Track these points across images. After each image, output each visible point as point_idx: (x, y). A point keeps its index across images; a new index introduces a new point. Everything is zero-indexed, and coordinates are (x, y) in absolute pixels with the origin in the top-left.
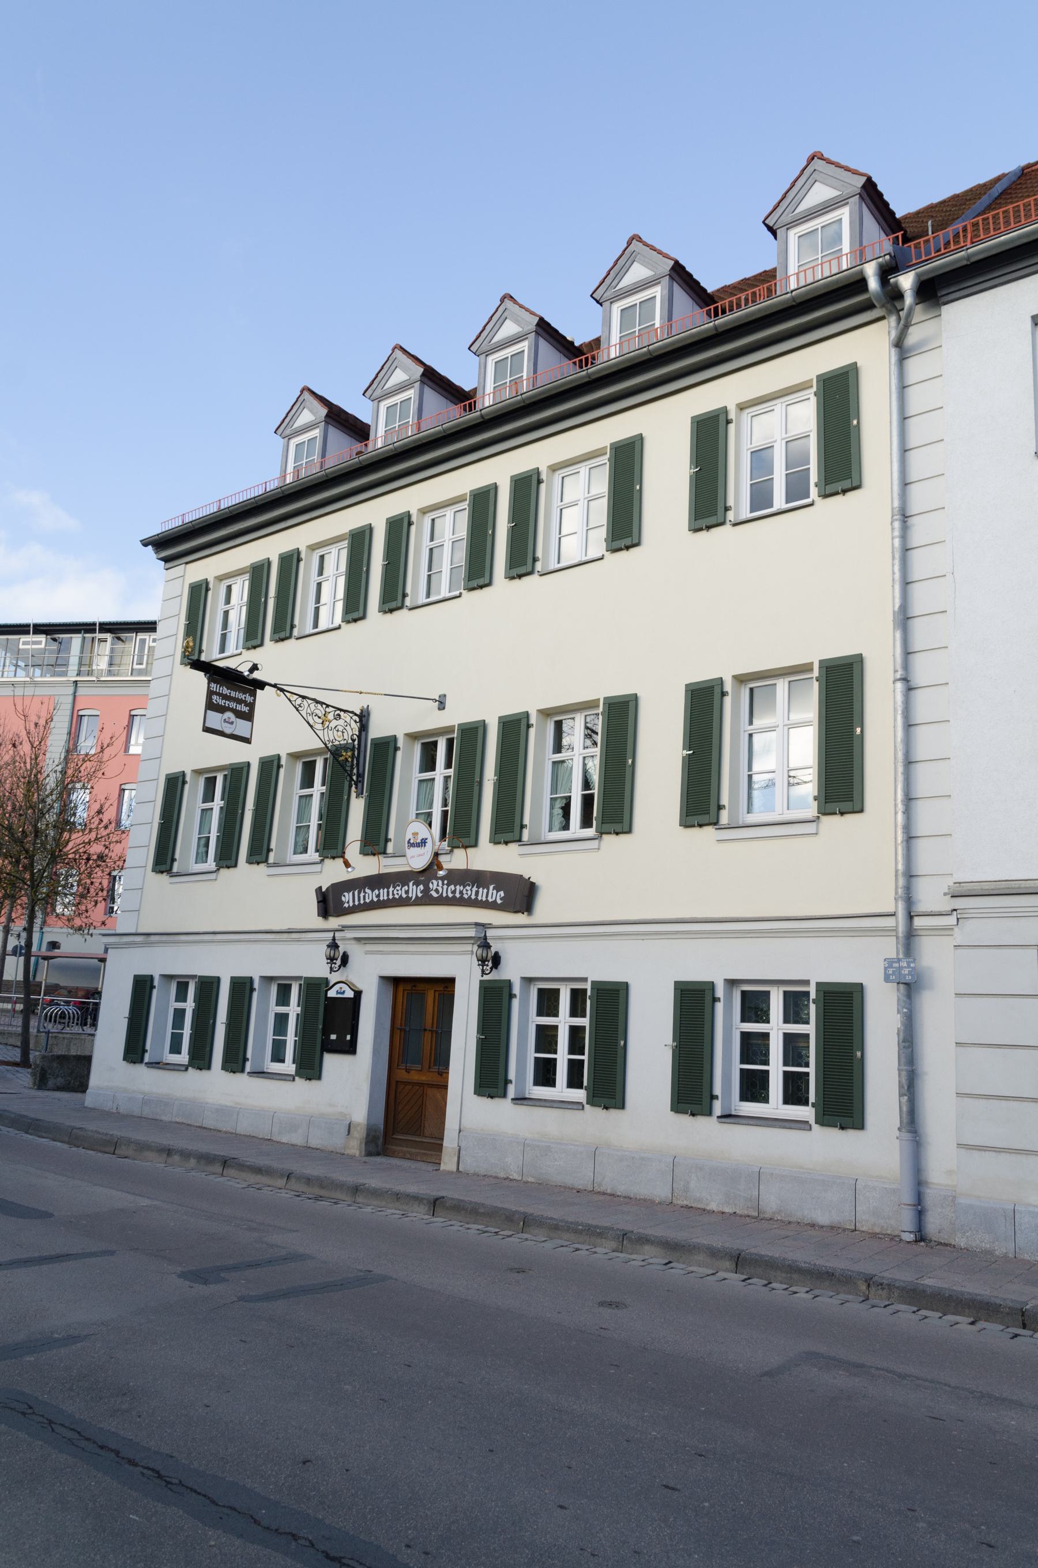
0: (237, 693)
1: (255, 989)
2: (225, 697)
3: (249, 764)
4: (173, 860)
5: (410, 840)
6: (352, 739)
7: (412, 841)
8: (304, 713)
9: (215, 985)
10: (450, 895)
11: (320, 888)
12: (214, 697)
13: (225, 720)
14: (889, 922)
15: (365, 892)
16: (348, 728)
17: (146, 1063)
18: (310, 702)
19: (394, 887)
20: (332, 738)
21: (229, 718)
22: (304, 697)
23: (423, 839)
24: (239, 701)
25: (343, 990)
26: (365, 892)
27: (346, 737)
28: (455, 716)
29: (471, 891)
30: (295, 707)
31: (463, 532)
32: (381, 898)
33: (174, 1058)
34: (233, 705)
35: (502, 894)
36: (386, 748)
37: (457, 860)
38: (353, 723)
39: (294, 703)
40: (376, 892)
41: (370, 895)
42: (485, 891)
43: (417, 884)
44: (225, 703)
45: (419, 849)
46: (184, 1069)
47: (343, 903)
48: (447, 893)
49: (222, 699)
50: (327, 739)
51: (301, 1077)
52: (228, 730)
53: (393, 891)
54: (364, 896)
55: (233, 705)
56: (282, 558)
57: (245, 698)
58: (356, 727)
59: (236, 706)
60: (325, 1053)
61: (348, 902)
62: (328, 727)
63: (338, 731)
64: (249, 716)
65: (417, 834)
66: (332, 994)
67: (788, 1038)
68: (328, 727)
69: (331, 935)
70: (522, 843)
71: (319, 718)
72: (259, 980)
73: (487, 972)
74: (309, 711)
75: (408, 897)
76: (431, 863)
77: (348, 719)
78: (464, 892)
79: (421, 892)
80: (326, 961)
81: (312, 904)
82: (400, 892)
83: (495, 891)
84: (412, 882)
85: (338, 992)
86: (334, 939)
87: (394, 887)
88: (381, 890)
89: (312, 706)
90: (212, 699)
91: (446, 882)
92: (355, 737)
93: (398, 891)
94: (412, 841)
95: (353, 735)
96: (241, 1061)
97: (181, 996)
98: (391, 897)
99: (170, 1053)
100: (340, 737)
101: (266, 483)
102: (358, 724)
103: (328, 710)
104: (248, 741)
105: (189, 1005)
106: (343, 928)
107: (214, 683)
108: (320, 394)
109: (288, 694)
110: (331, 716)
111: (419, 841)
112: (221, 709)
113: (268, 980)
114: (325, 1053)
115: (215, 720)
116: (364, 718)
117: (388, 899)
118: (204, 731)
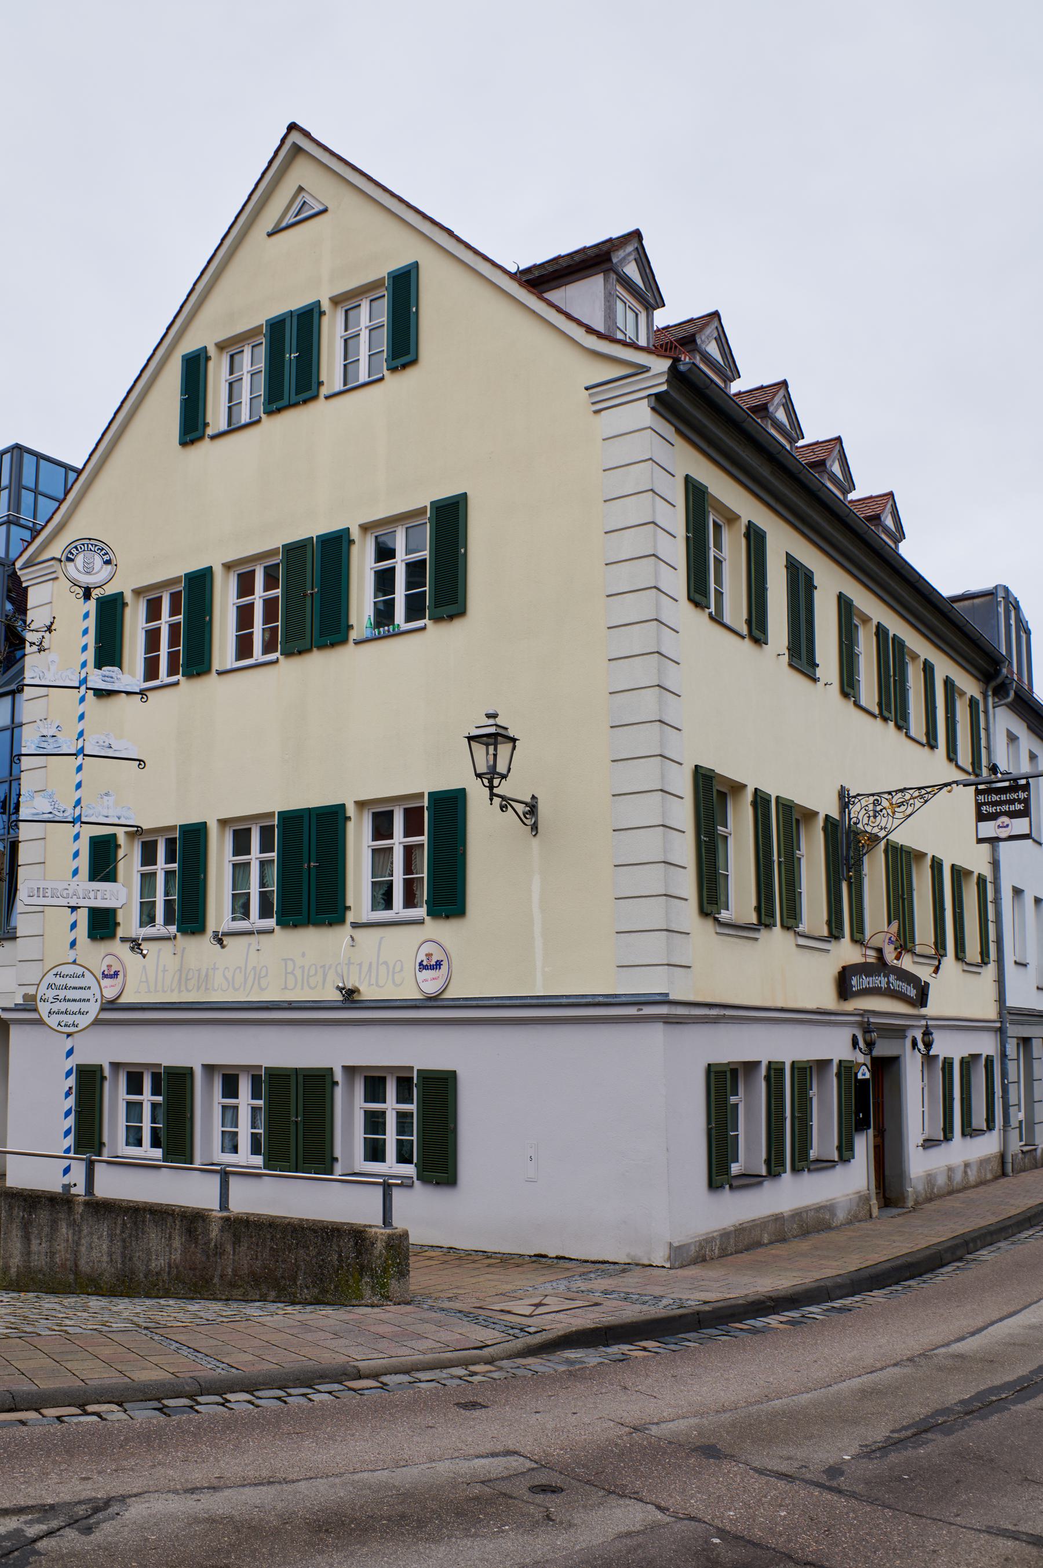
1: (106, 1077)
5: (422, 961)
13: (999, 826)
21: (1003, 823)
23: (438, 961)
30: (878, 794)
31: (383, 318)
34: (1005, 808)
44: (996, 810)
47: (852, 986)
55: (1005, 808)
57: (1018, 796)
59: (1009, 808)
67: (399, 1143)
97: (230, 1088)
107: (981, 795)
111: (433, 963)
112: (992, 817)
115: (988, 829)
118: (977, 843)
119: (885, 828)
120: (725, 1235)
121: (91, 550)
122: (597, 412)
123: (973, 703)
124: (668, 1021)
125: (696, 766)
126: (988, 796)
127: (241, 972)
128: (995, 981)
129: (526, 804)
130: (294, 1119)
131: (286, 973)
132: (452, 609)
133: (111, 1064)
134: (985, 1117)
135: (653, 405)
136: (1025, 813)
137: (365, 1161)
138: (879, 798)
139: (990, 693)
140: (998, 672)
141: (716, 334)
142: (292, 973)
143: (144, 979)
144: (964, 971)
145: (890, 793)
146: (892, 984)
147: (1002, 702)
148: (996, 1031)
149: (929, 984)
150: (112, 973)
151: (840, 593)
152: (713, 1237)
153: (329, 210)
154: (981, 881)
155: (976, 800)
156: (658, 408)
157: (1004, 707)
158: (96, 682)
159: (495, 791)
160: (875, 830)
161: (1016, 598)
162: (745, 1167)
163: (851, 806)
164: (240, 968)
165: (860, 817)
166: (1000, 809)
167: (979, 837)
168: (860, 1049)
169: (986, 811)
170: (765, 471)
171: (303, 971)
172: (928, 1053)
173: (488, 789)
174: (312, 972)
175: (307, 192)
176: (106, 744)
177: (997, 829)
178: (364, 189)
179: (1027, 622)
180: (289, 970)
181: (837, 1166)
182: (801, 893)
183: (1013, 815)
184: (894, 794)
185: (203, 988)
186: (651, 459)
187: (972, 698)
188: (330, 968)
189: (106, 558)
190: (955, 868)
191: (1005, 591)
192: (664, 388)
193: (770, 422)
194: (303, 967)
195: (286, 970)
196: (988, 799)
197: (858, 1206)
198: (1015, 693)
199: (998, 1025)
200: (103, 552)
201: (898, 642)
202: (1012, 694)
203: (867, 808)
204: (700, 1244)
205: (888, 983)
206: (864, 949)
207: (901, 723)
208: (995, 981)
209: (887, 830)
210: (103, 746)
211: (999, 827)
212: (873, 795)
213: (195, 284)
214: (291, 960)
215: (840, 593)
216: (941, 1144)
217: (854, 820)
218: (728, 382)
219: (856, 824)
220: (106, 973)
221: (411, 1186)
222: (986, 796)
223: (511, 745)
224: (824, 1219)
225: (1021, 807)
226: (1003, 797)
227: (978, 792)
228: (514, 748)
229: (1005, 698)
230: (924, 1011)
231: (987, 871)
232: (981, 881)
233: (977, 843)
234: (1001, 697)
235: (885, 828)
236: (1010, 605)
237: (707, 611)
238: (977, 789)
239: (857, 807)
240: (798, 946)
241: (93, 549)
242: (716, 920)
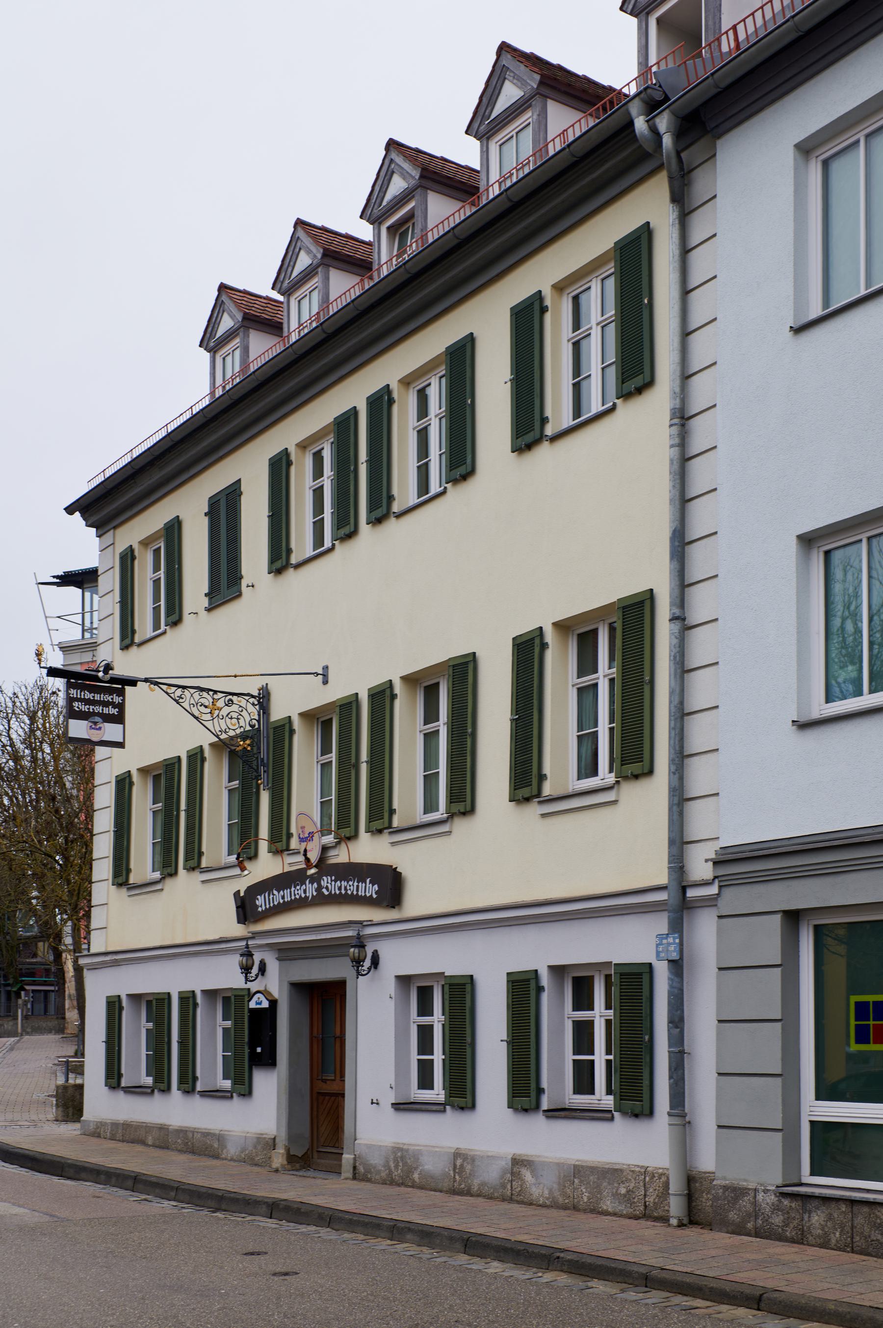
0: (102, 695)
2: (88, 702)
3: (179, 758)
4: (392, 812)
6: (250, 726)
8: (186, 705)
9: (646, 978)
10: (338, 892)
11: (239, 891)
12: (76, 704)
14: (662, 896)
16: (244, 713)
17: (544, 1111)
18: (192, 691)
19: (295, 887)
20: (224, 727)
22: (184, 687)
24: (106, 704)
25: (260, 1000)
26: (273, 895)
27: (242, 723)
28: (335, 692)
29: (353, 885)
30: (175, 700)
32: (286, 900)
33: (426, 1095)
34: (99, 709)
35: (376, 887)
36: (284, 730)
37: (340, 856)
38: (249, 705)
39: (172, 695)
40: (281, 893)
41: (277, 897)
42: (364, 885)
43: (312, 882)
44: (89, 709)
46: (149, 1090)
47: (257, 907)
48: (335, 890)
49: (85, 705)
50: (218, 729)
51: (624, 1113)
53: (294, 891)
54: (273, 898)
55: (99, 709)
56: (371, 403)
57: (112, 699)
58: (254, 711)
59: (103, 710)
60: (254, 1067)
61: (261, 906)
62: (218, 716)
63: (231, 718)
64: (119, 719)
66: (252, 1005)
68: (218, 716)
69: (244, 943)
70: (291, 852)
71: (206, 707)
72: (201, 995)
73: (363, 973)
74: (192, 702)
75: (306, 896)
76: (320, 858)
77: (243, 703)
78: (348, 888)
79: (316, 891)
80: (351, 964)
82: (352, 888)
83: (371, 885)
84: (308, 880)
85: (257, 1003)
86: (247, 946)
87: (295, 887)
88: (285, 891)
89: (196, 696)
90: (73, 706)
91: (333, 878)
92: (254, 721)
93: (298, 890)
95: (251, 720)
96: (533, 1094)
97: (583, 1000)
98: (293, 898)
99: (818, 1098)
100: (234, 725)
101: (734, 28)
102: (257, 707)
103: (216, 697)
104: (121, 745)
105: (437, 1019)
106: (255, 935)
107: (74, 689)
108: (527, 49)
109: (164, 687)
110: (221, 703)
113: (558, 971)
114: (254, 1067)
116: (263, 699)
120: (115, 1125)
136: (119, 719)
146: (327, 888)
150: (307, 835)
152: (106, 1123)
169: (78, 707)
177: (89, 730)
196: (81, 695)
197: (255, 1147)
204: (97, 1125)
220: (301, 836)
221: (612, 1119)
222: (79, 691)
224: (212, 1146)
226: (97, 697)
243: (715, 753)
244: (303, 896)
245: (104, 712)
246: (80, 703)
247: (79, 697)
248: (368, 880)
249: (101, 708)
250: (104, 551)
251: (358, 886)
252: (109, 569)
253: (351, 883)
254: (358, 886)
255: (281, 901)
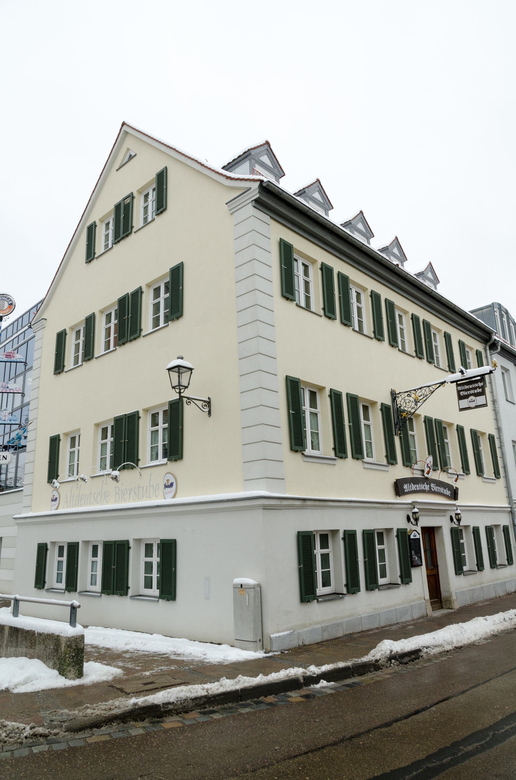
5: (165, 484)
7: (166, 485)
15: (411, 485)
21: (472, 399)
23: (171, 483)
26: (411, 485)
34: (472, 392)
41: (414, 487)
44: (468, 393)
45: (169, 488)
47: (404, 489)
52: (473, 405)
54: (411, 487)
55: (472, 392)
57: (478, 385)
59: (474, 392)
61: (406, 489)
65: (169, 480)
81: (391, 491)
87: (421, 484)
90: (460, 394)
94: (166, 485)
98: (420, 489)
107: (459, 386)
111: (169, 484)
112: (466, 397)
115: (464, 403)
117: (408, 491)
118: (460, 411)
119: (414, 408)
121: (3, 300)
122: (232, 214)
123: (478, 354)
124: (265, 508)
125: (287, 376)
126: (463, 387)
127: (100, 495)
128: (505, 487)
129: (204, 401)
130: (113, 567)
131: (116, 494)
132: (177, 315)
133: (51, 542)
134: (506, 558)
135: (254, 205)
137: (145, 588)
138: (410, 393)
139: (488, 348)
140: (490, 338)
141: (318, 189)
142: (118, 494)
143: (66, 501)
144: (483, 482)
145: (415, 390)
146: (433, 488)
147: (495, 352)
148: (509, 513)
149: (458, 488)
151: (386, 298)
153: (137, 155)
154: (491, 438)
155: (457, 389)
156: (256, 206)
157: (496, 354)
158: (3, 358)
159: (182, 395)
160: (409, 409)
161: (506, 309)
162: (335, 589)
163: (397, 399)
164: (99, 493)
165: (402, 404)
166: (470, 393)
167: (460, 408)
168: (412, 523)
169: (463, 394)
170: (329, 238)
171: (122, 492)
172: (459, 524)
173: (178, 394)
174: (125, 493)
175: (132, 151)
176: (6, 386)
178: (178, 159)
179: (514, 320)
180: (117, 492)
181: (400, 587)
182: (306, 430)
183: (476, 395)
184: (417, 390)
185: (86, 504)
186: (253, 230)
187: (477, 351)
188: (132, 490)
189: (10, 302)
190: (472, 430)
191: (499, 305)
192: (258, 196)
193: (353, 229)
194: (122, 490)
195: (116, 492)
198: (501, 347)
199: (510, 509)
200: (9, 300)
201: (426, 322)
202: (499, 348)
203: (404, 399)
205: (430, 488)
206: (412, 470)
207: (430, 360)
208: (505, 487)
209: (415, 409)
210: (5, 388)
211: (470, 402)
212: (407, 392)
213: (91, 197)
214: (118, 487)
215: (386, 298)
216: (476, 573)
217: (399, 405)
218: (327, 210)
219: (400, 407)
222: (462, 387)
223: (190, 372)
225: (480, 390)
226: (471, 386)
227: (458, 385)
228: (191, 373)
229: (496, 350)
230: (457, 503)
231: (494, 433)
232: (491, 438)
233: (460, 411)
234: (494, 350)
235: (414, 408)
236: (502, 311)
237: (295, 303)
238: (457, 384)
239: (400, 399)
240: (365, 468)
241: (4, 299)
242: (303, 454)
243: (281, 462)
244: (424, 489)
245: (475, 392)
246: (463, 392)
247: (462, 389)
248: (447, 489)
249: (473, 391)
250: (240, 328)
251: (444, 490)
252: (37, 388)
253: (441, 488)
254: (444, 490)
255: (415, 489)
